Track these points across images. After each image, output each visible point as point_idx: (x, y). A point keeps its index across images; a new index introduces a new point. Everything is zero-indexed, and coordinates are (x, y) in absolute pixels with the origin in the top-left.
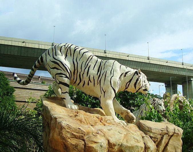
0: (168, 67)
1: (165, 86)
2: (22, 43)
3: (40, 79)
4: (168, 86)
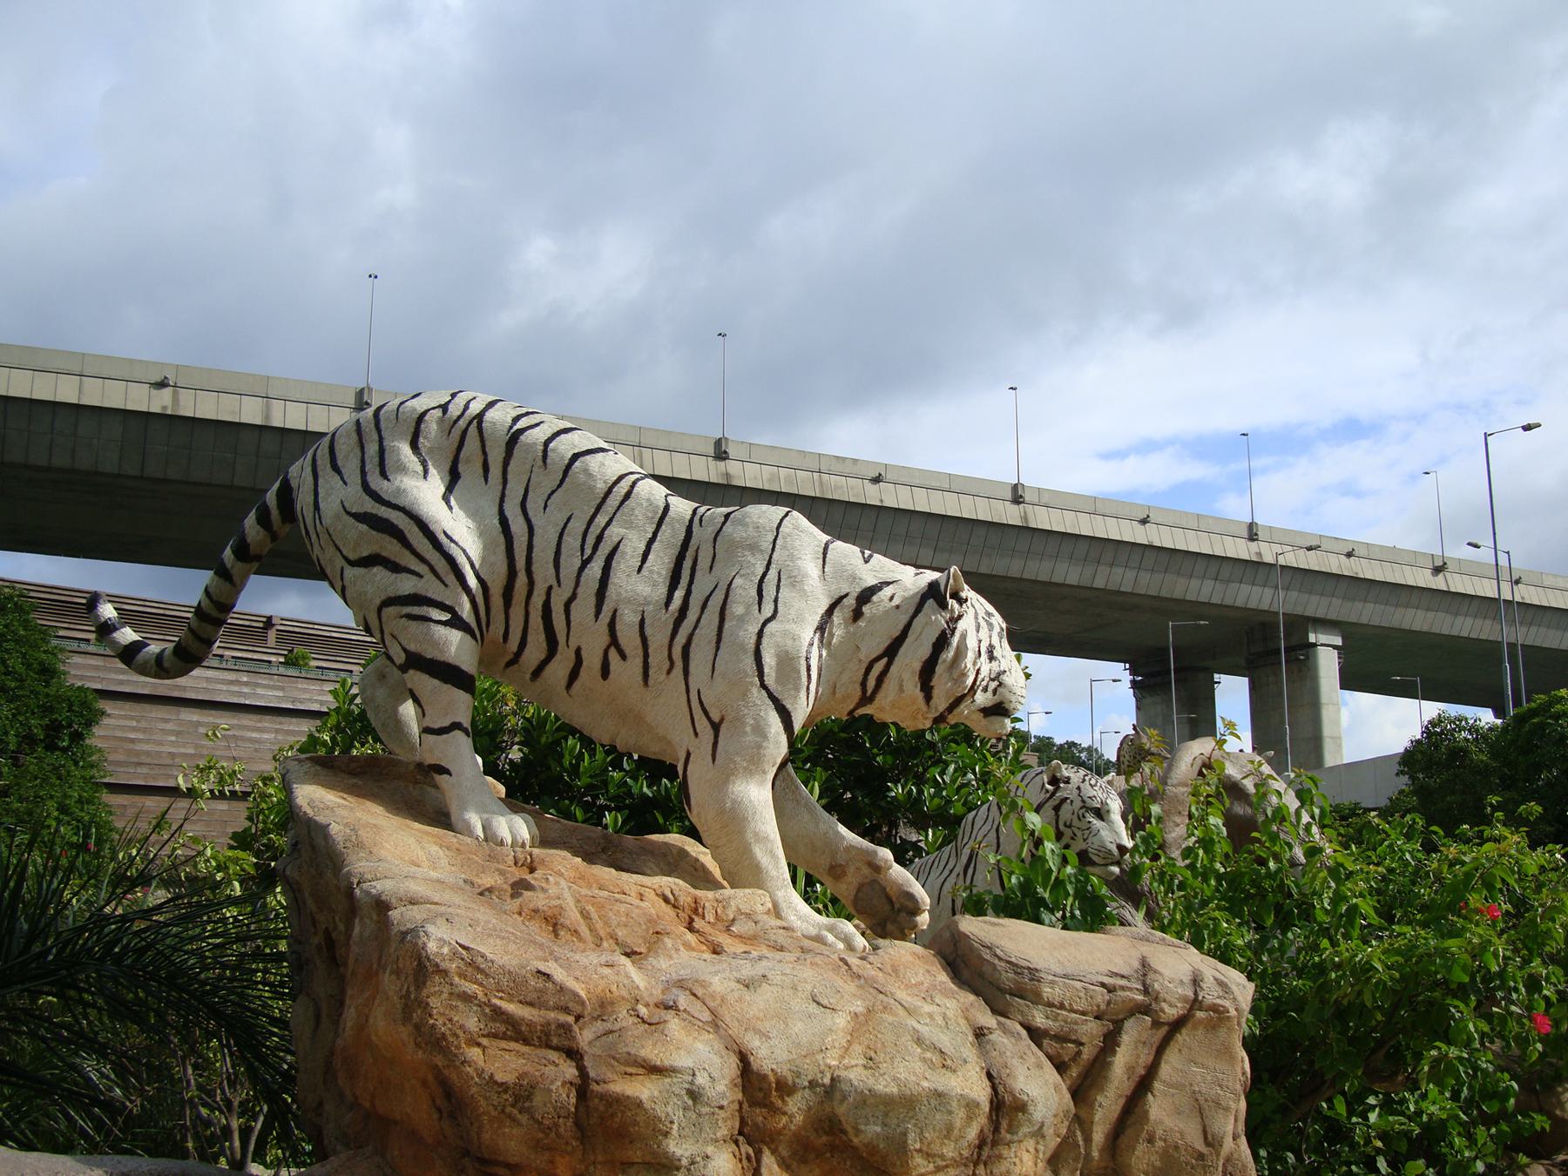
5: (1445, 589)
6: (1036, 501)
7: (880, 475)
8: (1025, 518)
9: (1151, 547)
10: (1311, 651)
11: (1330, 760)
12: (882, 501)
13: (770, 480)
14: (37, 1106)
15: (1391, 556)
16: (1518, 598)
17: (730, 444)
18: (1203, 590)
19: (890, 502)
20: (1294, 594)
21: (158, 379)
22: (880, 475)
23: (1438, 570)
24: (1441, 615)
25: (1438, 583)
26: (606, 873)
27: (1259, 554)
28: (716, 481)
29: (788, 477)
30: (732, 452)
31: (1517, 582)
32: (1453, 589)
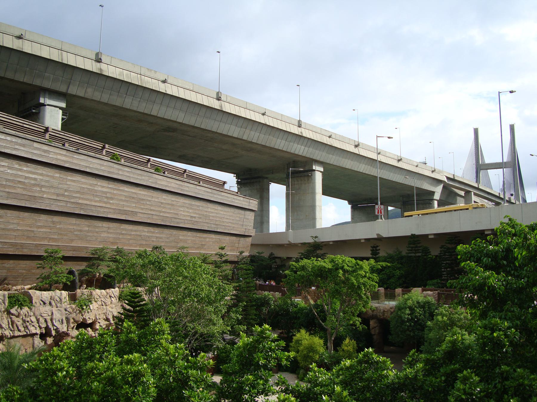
0: (307, 139)
1: (237, 182)
2: (15, 39)
3: (47, 136)
4: (355, 208)
5: (358, 153)
6: (225, 100)
7: (166, 79)
8: (221, 106)
9: (265, 125)
10: (313, 172)
11: (318, 226)
12: (166, 91)
13: (119, 75)
14: (502, 374)
15: (342, 139)
16: (379, 160)
17: (103, 55)
18: (280, 144)
19: (169, 92)
20: (311, 149)
21: (18, 34)
22: (166, 79)
23: (356, 146)
24: (356, 163)
25: (356, 151)
26: (32, 295)
27: (301, 133)
28: (95, 71)
29: (127, 75)
30: (104, 59)
31: (379, 154)
32: (361, 154)
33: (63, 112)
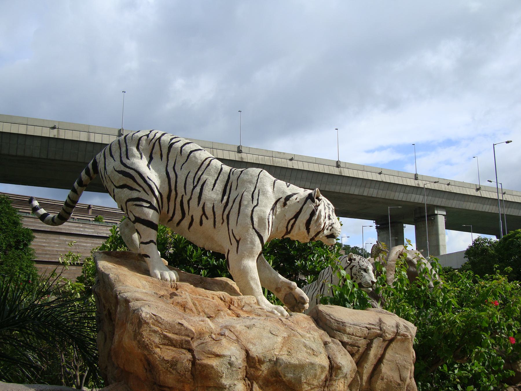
5: (480, 196)
6: (344, 167)
7: (292, 158)
8: (341, 172)
9: (382, 182)
10: (435, 216)
12: (293, 167)
13: (256, 160)
15: (462, 185)
16: (504, 199)
17: (243, 148)
18: (400, 196)
19: (296, 167)
20: (430, 198)
22: (292, 158)
23: (478, 190)
24: (479, 204)
25: (478, 194)
27: (418, 184)
28: (238, 160)
29: (262, 159)
30: (243, 150)
31: (504, 194)
32: (483, 196)
33: (445, 217)
